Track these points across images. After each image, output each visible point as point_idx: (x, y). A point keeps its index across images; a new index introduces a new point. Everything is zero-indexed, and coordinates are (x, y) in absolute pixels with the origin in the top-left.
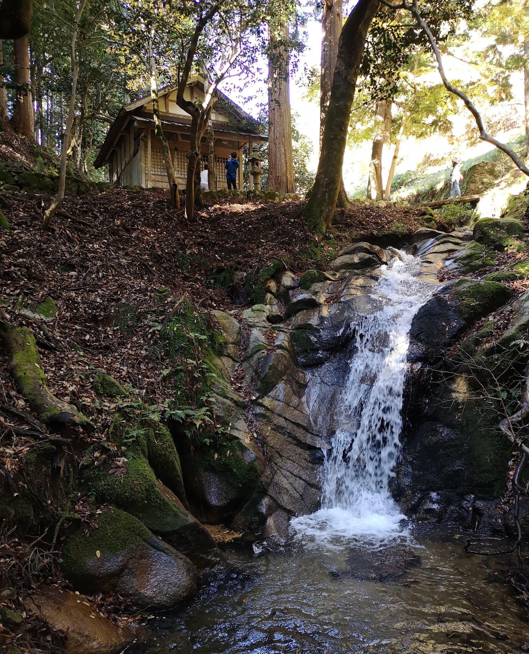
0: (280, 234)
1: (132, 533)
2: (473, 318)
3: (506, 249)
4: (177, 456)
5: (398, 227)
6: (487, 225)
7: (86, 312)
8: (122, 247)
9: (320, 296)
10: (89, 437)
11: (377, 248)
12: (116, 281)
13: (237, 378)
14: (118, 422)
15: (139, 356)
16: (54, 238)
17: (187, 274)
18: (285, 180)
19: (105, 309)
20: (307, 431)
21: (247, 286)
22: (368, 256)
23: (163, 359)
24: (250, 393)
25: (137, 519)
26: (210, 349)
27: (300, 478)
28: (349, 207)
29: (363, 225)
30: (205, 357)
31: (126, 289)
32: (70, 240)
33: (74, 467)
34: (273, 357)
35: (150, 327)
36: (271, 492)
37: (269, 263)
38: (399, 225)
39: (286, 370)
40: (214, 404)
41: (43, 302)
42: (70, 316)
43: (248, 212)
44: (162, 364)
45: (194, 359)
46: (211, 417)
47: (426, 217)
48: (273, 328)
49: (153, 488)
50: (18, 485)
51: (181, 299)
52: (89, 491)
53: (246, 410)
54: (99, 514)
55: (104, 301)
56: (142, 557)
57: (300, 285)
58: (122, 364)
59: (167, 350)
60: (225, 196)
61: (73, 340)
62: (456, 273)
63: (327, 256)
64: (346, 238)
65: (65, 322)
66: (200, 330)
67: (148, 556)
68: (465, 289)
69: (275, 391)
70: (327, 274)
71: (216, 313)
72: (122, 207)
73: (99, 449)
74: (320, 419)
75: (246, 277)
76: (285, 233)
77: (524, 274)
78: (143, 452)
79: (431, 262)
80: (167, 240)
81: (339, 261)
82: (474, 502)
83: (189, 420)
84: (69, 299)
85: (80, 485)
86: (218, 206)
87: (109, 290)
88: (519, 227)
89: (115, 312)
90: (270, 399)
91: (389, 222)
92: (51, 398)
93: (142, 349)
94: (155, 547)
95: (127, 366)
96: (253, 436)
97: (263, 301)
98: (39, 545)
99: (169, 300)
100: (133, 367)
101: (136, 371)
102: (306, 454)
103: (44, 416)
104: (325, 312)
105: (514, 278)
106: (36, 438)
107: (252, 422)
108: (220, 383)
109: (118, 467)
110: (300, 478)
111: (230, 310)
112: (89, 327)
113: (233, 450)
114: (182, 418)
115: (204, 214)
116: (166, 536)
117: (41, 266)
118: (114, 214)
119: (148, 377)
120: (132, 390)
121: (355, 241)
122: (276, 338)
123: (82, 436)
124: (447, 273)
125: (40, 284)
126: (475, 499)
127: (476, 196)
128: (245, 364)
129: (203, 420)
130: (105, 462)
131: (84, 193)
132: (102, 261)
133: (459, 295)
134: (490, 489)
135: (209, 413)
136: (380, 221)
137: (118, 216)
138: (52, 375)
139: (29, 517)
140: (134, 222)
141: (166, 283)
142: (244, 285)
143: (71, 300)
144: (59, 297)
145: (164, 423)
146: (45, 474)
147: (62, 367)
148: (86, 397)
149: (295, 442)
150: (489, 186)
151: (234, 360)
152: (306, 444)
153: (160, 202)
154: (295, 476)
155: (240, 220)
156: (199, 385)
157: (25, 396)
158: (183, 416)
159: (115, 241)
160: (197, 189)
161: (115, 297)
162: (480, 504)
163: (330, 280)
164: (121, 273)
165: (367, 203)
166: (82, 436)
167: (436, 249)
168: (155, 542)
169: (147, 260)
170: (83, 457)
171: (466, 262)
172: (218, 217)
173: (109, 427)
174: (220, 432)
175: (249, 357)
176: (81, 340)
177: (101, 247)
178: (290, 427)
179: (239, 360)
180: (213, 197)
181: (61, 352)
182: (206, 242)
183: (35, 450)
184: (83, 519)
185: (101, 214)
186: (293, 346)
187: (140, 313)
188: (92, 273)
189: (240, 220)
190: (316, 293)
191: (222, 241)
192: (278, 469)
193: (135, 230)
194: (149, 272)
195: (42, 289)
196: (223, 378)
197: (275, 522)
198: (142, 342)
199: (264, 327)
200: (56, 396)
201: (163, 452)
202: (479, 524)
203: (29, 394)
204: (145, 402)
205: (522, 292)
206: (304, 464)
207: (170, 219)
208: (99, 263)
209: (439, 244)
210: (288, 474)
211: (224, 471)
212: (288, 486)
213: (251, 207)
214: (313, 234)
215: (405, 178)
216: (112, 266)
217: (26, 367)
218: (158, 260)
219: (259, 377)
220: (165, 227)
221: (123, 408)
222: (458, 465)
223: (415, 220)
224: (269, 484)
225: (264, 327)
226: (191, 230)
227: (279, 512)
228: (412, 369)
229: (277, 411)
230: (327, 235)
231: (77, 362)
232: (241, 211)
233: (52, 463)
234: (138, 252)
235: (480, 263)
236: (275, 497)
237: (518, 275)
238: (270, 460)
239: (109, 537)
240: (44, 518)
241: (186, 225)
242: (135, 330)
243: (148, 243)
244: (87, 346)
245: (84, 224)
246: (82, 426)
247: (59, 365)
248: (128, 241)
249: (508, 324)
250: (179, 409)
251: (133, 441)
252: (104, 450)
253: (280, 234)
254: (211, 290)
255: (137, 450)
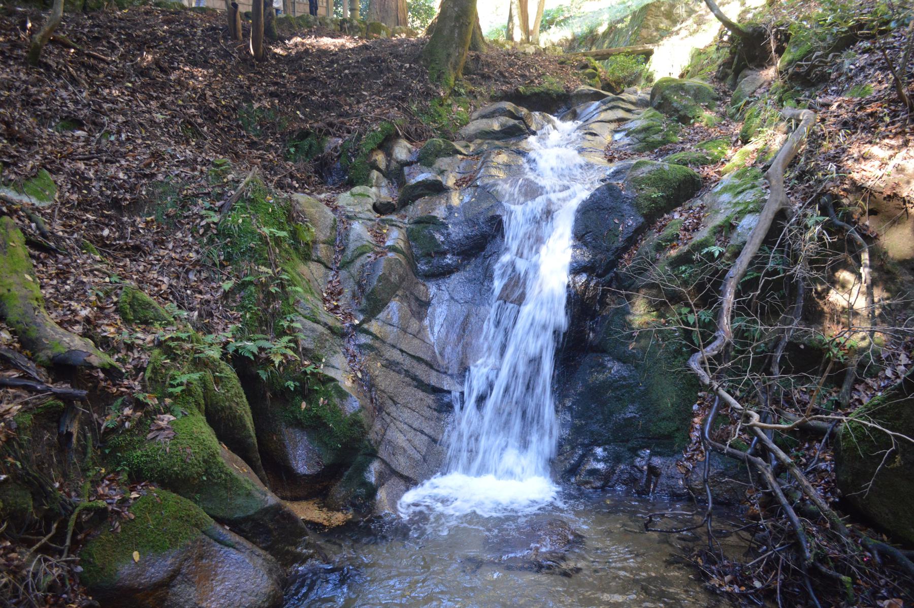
0: (390, 85)
1: (186, 524)
2: (653, 215)
3: (692, 121)
4: (248, 408)
5: (552, 83)
6: (669, 88)
7: (102, 193)
8: (155, 95)
9: (448, 177)
10: (114, 385)
11: (524, 111)
12: (148, 146)
13: (331, 293)
14: (159, 363)
15: (186, 260)
16: (49, 77)
17: (255, 139)
18: (394, 7)
19: (132, 190)
20: (431, 367)
21: (343, 159)
22: (512, 122)
23: (223, 266)
24: (350, 314)
25: (192, 503)
26: (291, 251)
27: (422, 432)
28: (486, 51)
29: (505, 77)
30: (284, 263)
31: (164, 159)
32: (74, 81)
33: (92, 430)
34: (383, 262)
35: (202, 218)
36: (383, 453)
37: (375, 127)
38: (554, 80)
39: (401, 283)
40: (300, 331)
41: (35, 177)
42: (78, 199)
43: (342, 49)
44: (222, 274)
45: (270, 266)
46: (295, 350)
47: (588, 71)
48: (383, 221)
49: (215, 457)
50: (5, 462)
51: (249, 177)
52: (118, 465)
53: (346, 340)
54: (135, 499)
55: (129, 177)
56: (201, 557)
57: (419, 160)
58: (161, 273)
59: (228, 252)
60: (309, 25)
61: (84, 237)
62: (629, 151)
63: (457, 119)
64: (481, 94)
65: (70, 208)
66: (277, 223)
67: (210, 555)
68: (644, 175)
69: (386, 312)
70: (457, 146)
71: (298, 197)
72: (153, 34)
73: (131, 403)
74: (448, 349)
75: (342, 146)
76: (396, 83)
77: (716, 157)
78: (198, 405)
79: (595, 135)
80: (224, 87)
81: (473, 127)
82: (650, 459)
83: (263, 355)
84: (75, 173)
85: (104, 457)
86: (299, 39)
87: (137, 160)
88: (709, 93)
89: (147, 194)
90: (380, 323)
91: (539, 76)
92: (52, 328)
93: (190, 251)
94: (220, 542)
95: (169, 276)
96: (356, 376)
97: (366, 181)
98: (44, 549)
99: (230, 177)
100: (178, 278)
101: (182, 284)
102: (430, 399)
103: (43, 356)
104: (455, 200)
105: (704, 162)
106: (30, 390)
107: (355, 356)
108: (308, 300)
109: (162, 429)
110: (422, 432)
111: (319, 194)
112: (107, 216)
113: (328, 396)
114: (253, 353)
115: (278, 51)
116: (236, 526)
117: (30, 121)
118: (143, 45)
119: (200, 293)
120: (177, 312)
121: (494, 99)
122: (387, 235)
123: (103, 384)
124: (617, 150)
125: (29, 149)
126: (651, 455)
127: (650, 47)
128: (343, 274)
129: (284, 355)
130: (140, 422)
131: (93, 10)
132: (125, 115)
133: (637, 183)
134: (667, 442)
135: (292, 345)
136: (528, 74)
137: (148, 47)
138: (52, 291)
139: (27, 509)
140: (172, 57)
141: (224, 151)
142: (339, 157)
143: (78, 174)
144: (59, 170)
145: (227, 361)
146: (47, 444)
147: (68, 279)
148: (107, 325)
149: (415, 383)
150: (667, 33)
151: (326, 267)
152: (429, 385)
153: (212, 29)
154: (415, 429)
155: (332, 62)
156: (278, 305)
157: (10, 324)
158: (256, 351)
159: (144, 85)
160: (268, 11)
161: (148, 172)
162: (657, 461)
163: (461, 153)
164: (155, 135)
165: (508, 47)
166: (103, 384)
167: (603, 116)
168: (220, 534)
169: (194, 116)
170: (106, 416)
171: (641, 136)
172: (300, 56)
173: (144, 370)
174: (309, 372)
175: (348, 263)
176: (96, 236)
177: (123, 93)
178: (407, 363)
179: (334, 267)
180: (291, 26)
181: (65, 255)
182: (282, 92)
183: (31, 409)
184: (110, 508)
185: (121, 43)
186: (410, 247)
187: (186, 196)
188: (110, 133)
189: (332, 62)
190: (442, 172)
191: (306, 91)
192: (392, 421)
193: (174, 69)
194: (198, 134)
195: (32, 156)
196: (312, 293)
197: (388, 494)
198: (191, 239)
199: (370, 220)
200: (60, 324)
201: (227, 404)
202: (655, 486)
203: (18, 322)
204: (198, 330)
205: (715, 182)
206: (428, 413)
207: (227, 55)
208: (121, 119)
209: (606, 110)
210: (405, 427)
211: (315, 426)
212: (405, 444)
213: (346, 42)
214: (437, 86)
215: (555, 15)
216: (141, 124)
217: (11, 281)
218: (211, 115)
219: (363, 292)
220: (221, 67)
221: (165, 341)
222: (631, 411)
223: (574, 74)
224: (380, 442)
225: (370, 220)
226: (259, 73)
227: (394, 481)
228: (574, 283)
229: (389, 341)
230: (456, 88)
231: (91, 271)
232: (332, 48)
233: (59, 427)
234: (180, 102)
235: (660, 138)
236: (388, 460)
237: (710, 158)
238: (380, 409)
239: (152, 532)
240: (51, 510)
241: (253, 65)
242: (179, 222)
243: (194, 90)
244: (106, 245)
245: (95, 57)
246: (104, 370)
247: (62, 275)
248: (164, 86)
249: (698, 224)
250: (249, 340)
251: (182, 391)
252: (139, 405)
253: (390, 85)
254: (290, 163)
255: (188, 403)
